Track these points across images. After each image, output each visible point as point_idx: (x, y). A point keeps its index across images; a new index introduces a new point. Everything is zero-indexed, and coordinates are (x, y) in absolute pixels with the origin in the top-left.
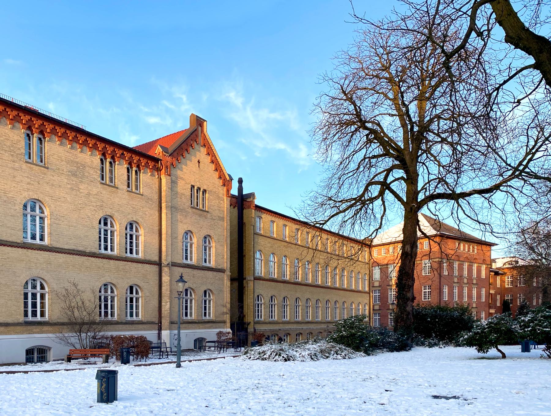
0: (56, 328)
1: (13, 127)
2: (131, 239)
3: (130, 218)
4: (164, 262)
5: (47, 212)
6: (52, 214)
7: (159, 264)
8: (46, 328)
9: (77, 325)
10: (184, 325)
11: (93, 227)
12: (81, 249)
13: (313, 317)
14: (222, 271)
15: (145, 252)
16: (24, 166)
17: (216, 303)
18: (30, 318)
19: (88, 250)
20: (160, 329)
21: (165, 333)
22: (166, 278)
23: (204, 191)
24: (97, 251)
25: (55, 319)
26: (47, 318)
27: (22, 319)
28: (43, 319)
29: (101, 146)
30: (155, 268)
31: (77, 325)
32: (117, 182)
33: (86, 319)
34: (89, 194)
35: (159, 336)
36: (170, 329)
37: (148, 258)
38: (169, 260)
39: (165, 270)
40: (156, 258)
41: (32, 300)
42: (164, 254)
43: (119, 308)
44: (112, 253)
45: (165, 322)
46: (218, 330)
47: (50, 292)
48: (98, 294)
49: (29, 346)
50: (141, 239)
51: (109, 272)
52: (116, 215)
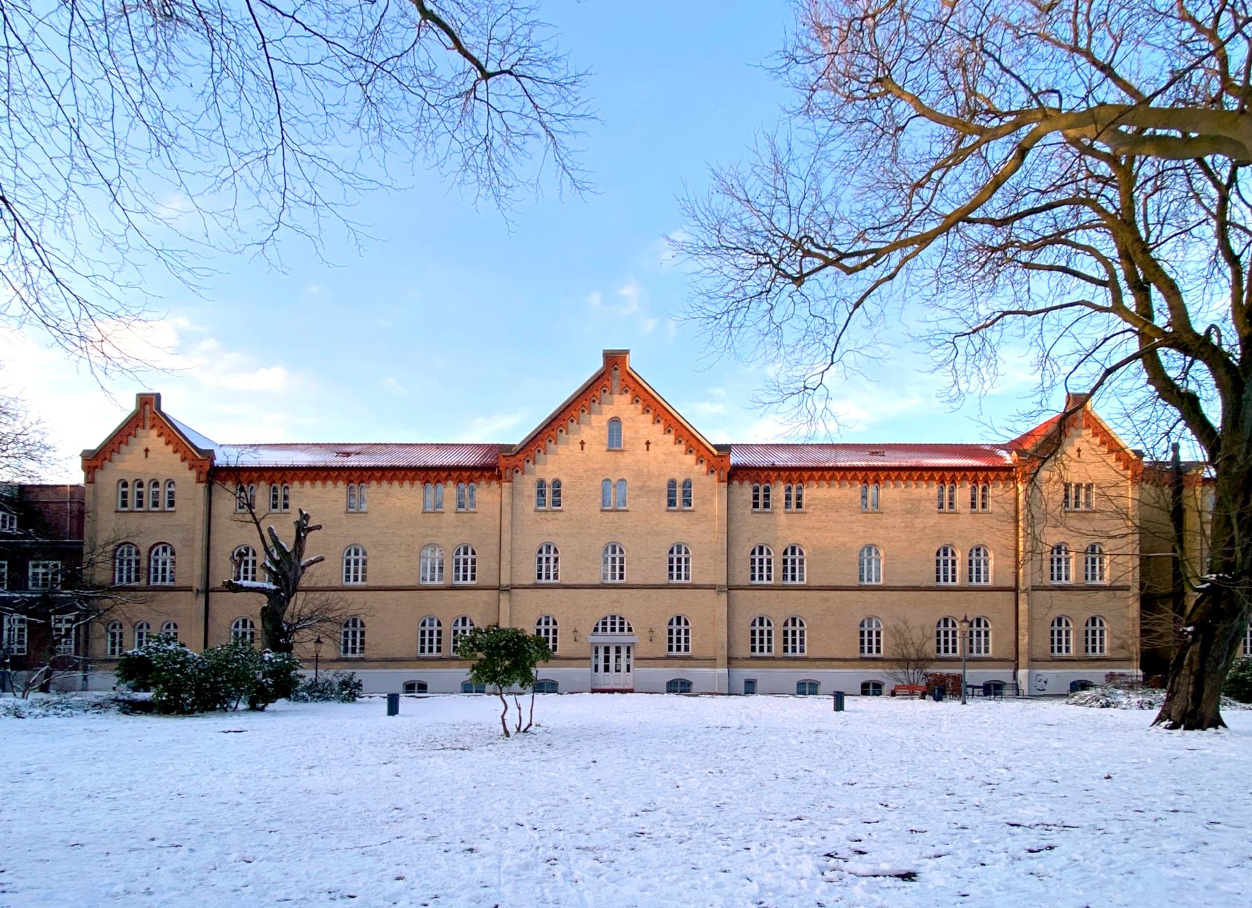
0: (886, 664)
1: (852, 485)
2: (974, 569)
3: (975, 543)
4: (1021, 587)
5: (882, 553)
6: (886, 555)
7: (1015, 590)
8: (880, 664)
9: (904, 661)
10: (971, 663)
11: (930, 561)
12: (916, 584)
13: (963, 650)
14: (1127, 588)
15: (994, 579)
16: (860, 517)
17: (1110, 633)
18: (866, 654)
19: (924, 585)
20: (1017, 668)
21: (1022, 673)
22: (1023, 607)
23: (1089, 487)
24: (935, 584)
25: (889, 656)
26: (882, 654)
27: (858, 655)
28: (878, 655)
29: (937, 475)
30: (1011, 595)
31: (904, 661)
32: (957, 506)
33: (914, 656)
34: (925, 528)
35: (1015, 677)
36: (1029, 667)
37: (999, 584)
38: (1029, 584)
39: (1022, 596)
40: (1012, 584)
41: (867, 638)
42: (1021, 579)
43: (1076, 644)
44: (1067, 583)
45: (1023, 659)
46: (1108, 671)
47: (885, 629)
48: (1084, 629)
49: (864, 680)
50: (991, 563)
51: (948, 605)
52: (957, 542)
